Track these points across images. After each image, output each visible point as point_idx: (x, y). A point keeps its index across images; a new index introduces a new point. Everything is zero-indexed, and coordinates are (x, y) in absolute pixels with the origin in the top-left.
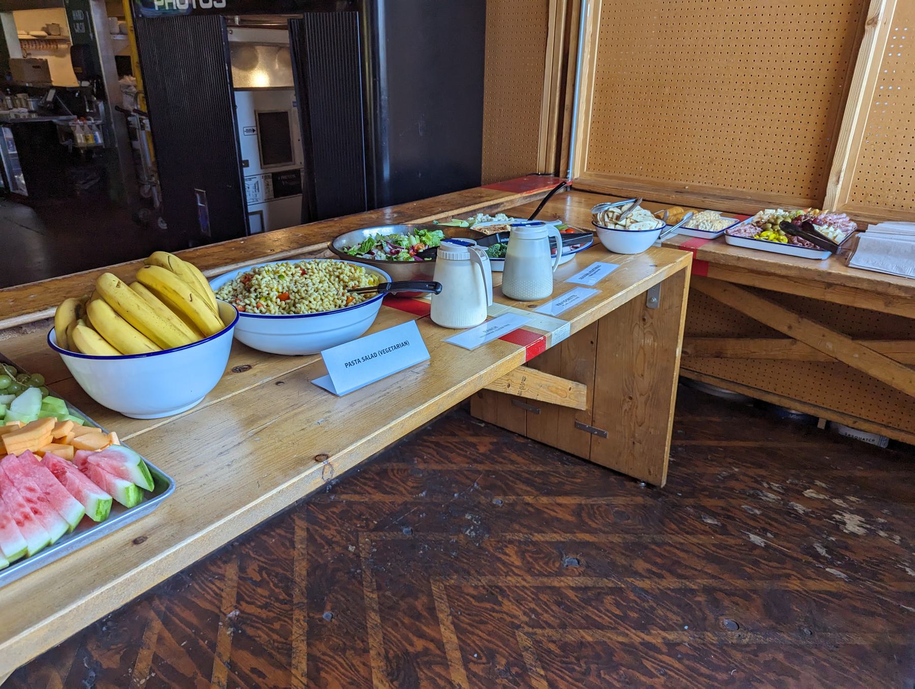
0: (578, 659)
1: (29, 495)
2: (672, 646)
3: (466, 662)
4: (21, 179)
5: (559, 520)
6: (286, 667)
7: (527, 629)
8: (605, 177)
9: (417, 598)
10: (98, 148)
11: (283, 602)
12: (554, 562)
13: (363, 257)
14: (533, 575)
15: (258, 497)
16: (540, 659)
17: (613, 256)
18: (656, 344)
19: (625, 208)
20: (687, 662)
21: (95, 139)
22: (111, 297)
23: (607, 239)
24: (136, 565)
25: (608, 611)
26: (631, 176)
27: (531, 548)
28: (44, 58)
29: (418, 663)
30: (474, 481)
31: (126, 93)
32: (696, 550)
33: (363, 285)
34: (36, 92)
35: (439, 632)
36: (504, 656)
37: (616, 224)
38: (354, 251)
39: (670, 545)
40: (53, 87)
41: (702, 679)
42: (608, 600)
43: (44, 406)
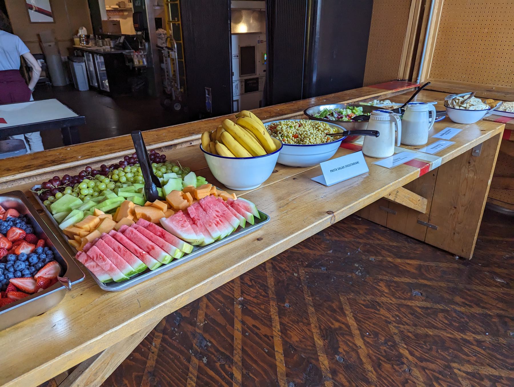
0: (425, 342)
1: (217, 214)
2: (479, 343)
3: (363, 336)
4: (106, 83)
5: (408, 272)
6: (270, 327)
7: (394, 324)
8: (440, 81)
9: (333, 302)
10: (144, 67)
11: (264, 296)
12: (407, 293)
13: (324, 118)
14: (396, 298)
15: (306, 227)
16: (403, 339)
17: (456, 125)
18: (475, 177)
19: (466, 97)
20: (489, 352)
21: (143, 63)
22: (232, 131)
23: (453, 115)
24: (263, 249)
25: (440, 320)
26: (457, 81)
27: (393, 284)
28: (118, 19)
29: (337, 334)
30: (358, 248)
31: (159, 38)
32: (491, 294)
33: (331, 133)
34: (114, 37)
35: (347, 320)
36: (383, 336)
37: (460, 106)
38: (317, 115)
39: (476, 290)
40: (123, 35)
41: (498, 361)
42: (441, 315)
43: (198, 180)
